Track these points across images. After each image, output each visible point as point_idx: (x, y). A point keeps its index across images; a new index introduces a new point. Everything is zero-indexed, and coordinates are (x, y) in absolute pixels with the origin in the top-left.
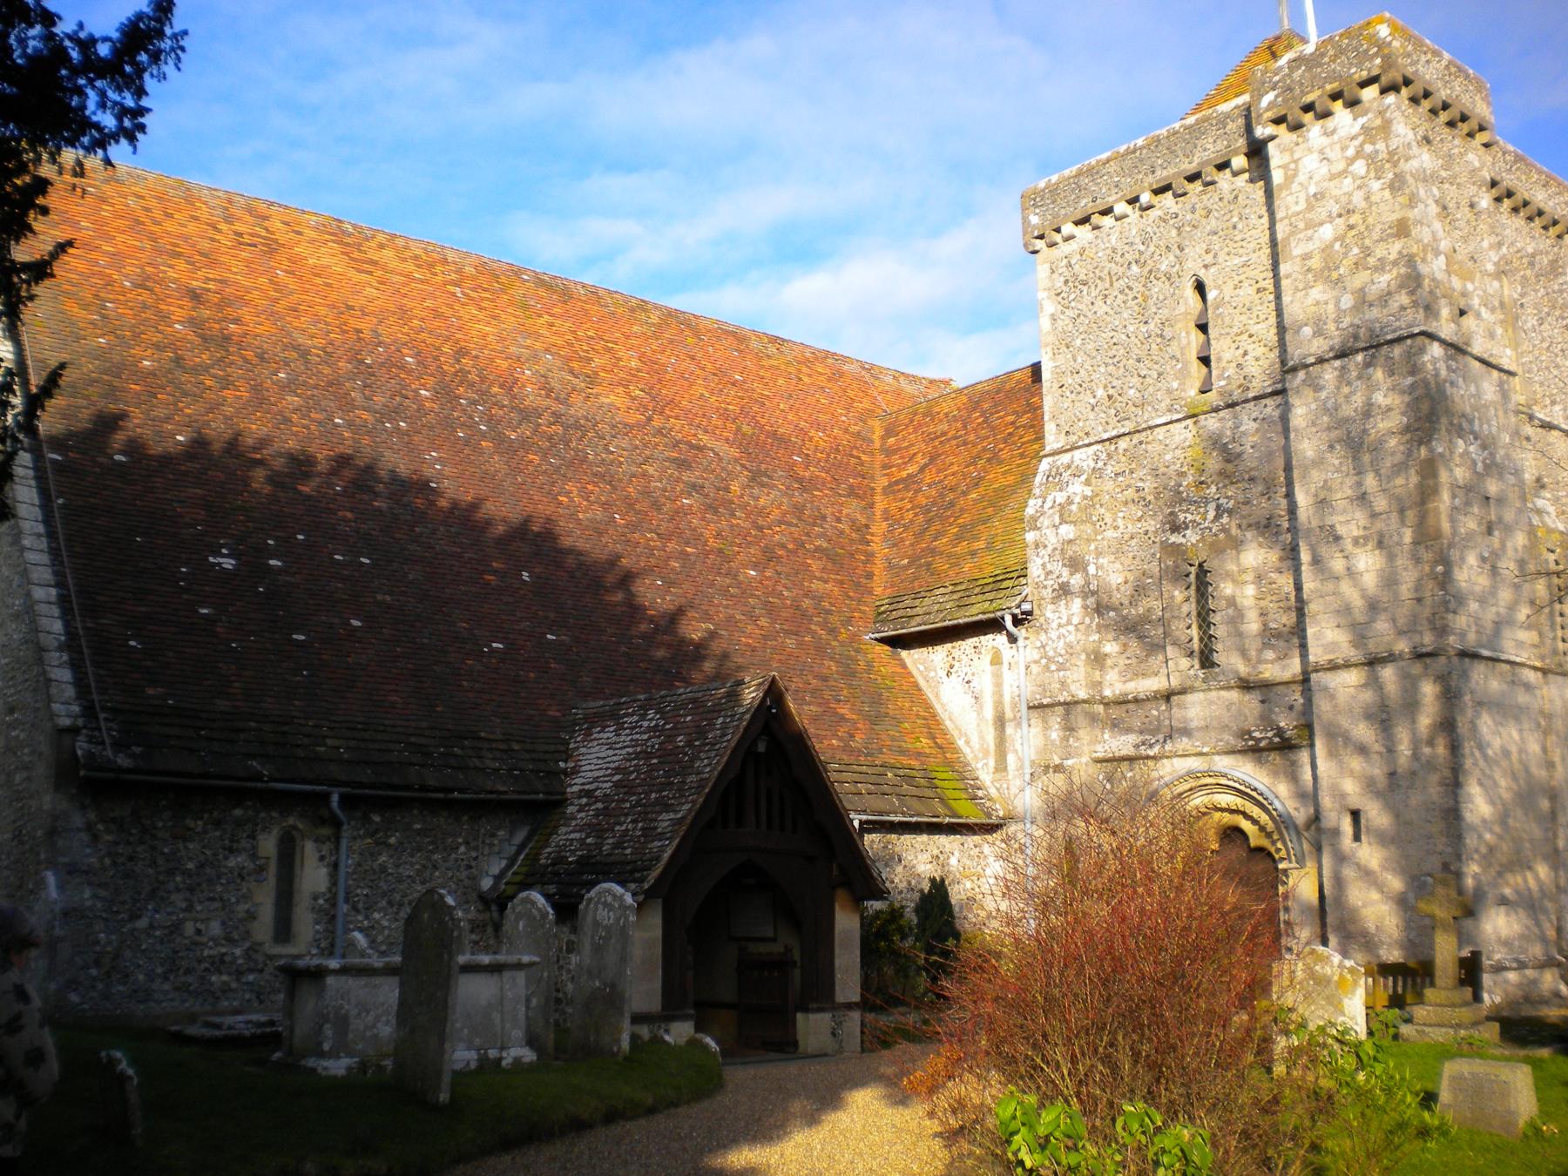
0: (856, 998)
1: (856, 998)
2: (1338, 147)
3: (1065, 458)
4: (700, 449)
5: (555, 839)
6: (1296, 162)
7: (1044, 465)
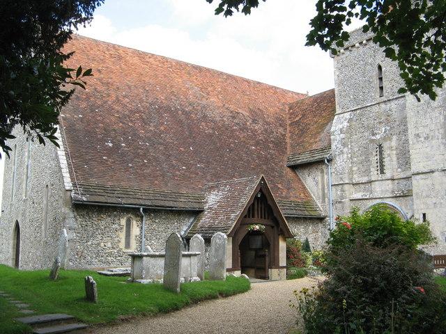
0: (285, 265)
1: (285, 265)
3: (342, 115)
4: (238, 113)
5: (201, 221)
7: (336, 117)
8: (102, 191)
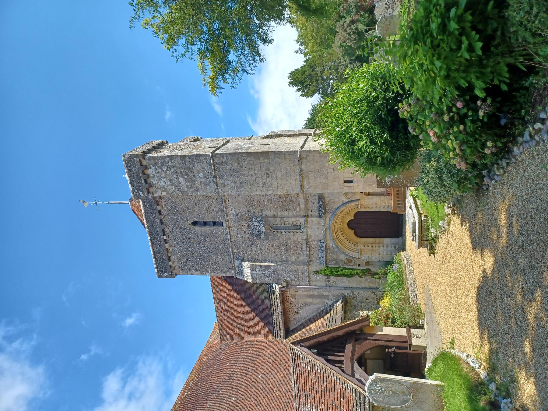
6: (161, 188)
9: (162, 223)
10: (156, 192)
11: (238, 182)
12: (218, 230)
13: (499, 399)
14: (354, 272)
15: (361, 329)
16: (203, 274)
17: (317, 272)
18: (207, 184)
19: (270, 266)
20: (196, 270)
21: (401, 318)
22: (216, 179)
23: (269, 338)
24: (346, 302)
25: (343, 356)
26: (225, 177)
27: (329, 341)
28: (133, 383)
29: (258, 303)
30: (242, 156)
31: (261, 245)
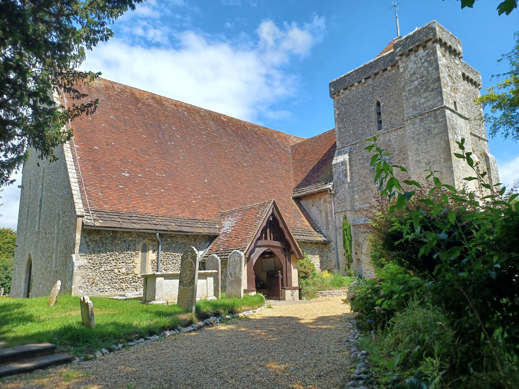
2: (419, 60)
8: (117, 217)
9: (376, 74)
10: (403, 63)
11: (419, 136)
12: (374, 127)
13: (220, 318)
14: (348, 248)
15: (293, 253)
16: (335, 121)
17: (345, 218)
18: (414, 108)
19: (347, 177)
20: (338, 115)
21: (307, 284)
22: (419, 116)
23: (293, 185)
24: (325, 244)
25: (271, 240)
26: (423, 124)
27: (280, 229)
28: (277, 75)
29: (318, 172)
30: (445, 136)
31: (364, 167)
